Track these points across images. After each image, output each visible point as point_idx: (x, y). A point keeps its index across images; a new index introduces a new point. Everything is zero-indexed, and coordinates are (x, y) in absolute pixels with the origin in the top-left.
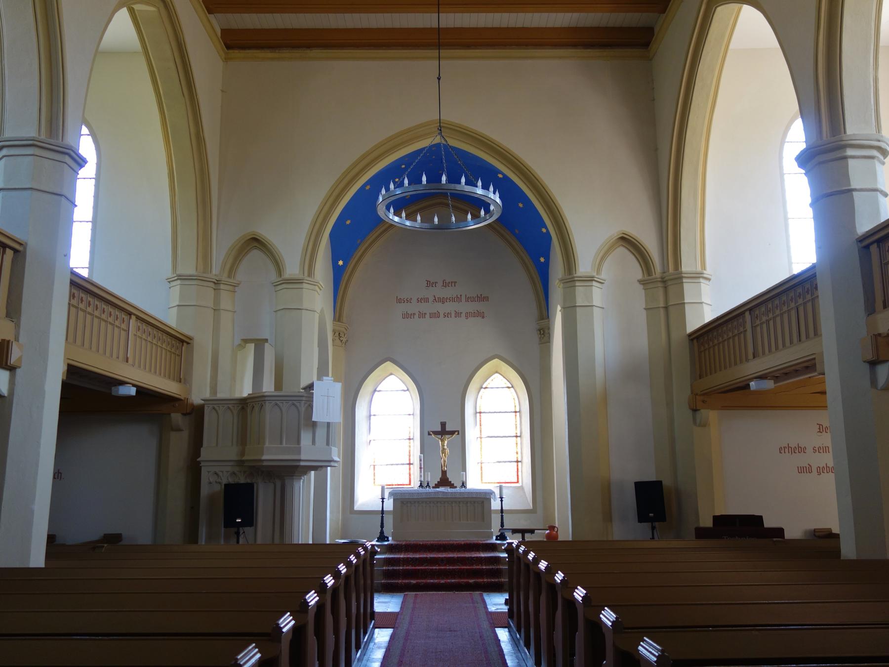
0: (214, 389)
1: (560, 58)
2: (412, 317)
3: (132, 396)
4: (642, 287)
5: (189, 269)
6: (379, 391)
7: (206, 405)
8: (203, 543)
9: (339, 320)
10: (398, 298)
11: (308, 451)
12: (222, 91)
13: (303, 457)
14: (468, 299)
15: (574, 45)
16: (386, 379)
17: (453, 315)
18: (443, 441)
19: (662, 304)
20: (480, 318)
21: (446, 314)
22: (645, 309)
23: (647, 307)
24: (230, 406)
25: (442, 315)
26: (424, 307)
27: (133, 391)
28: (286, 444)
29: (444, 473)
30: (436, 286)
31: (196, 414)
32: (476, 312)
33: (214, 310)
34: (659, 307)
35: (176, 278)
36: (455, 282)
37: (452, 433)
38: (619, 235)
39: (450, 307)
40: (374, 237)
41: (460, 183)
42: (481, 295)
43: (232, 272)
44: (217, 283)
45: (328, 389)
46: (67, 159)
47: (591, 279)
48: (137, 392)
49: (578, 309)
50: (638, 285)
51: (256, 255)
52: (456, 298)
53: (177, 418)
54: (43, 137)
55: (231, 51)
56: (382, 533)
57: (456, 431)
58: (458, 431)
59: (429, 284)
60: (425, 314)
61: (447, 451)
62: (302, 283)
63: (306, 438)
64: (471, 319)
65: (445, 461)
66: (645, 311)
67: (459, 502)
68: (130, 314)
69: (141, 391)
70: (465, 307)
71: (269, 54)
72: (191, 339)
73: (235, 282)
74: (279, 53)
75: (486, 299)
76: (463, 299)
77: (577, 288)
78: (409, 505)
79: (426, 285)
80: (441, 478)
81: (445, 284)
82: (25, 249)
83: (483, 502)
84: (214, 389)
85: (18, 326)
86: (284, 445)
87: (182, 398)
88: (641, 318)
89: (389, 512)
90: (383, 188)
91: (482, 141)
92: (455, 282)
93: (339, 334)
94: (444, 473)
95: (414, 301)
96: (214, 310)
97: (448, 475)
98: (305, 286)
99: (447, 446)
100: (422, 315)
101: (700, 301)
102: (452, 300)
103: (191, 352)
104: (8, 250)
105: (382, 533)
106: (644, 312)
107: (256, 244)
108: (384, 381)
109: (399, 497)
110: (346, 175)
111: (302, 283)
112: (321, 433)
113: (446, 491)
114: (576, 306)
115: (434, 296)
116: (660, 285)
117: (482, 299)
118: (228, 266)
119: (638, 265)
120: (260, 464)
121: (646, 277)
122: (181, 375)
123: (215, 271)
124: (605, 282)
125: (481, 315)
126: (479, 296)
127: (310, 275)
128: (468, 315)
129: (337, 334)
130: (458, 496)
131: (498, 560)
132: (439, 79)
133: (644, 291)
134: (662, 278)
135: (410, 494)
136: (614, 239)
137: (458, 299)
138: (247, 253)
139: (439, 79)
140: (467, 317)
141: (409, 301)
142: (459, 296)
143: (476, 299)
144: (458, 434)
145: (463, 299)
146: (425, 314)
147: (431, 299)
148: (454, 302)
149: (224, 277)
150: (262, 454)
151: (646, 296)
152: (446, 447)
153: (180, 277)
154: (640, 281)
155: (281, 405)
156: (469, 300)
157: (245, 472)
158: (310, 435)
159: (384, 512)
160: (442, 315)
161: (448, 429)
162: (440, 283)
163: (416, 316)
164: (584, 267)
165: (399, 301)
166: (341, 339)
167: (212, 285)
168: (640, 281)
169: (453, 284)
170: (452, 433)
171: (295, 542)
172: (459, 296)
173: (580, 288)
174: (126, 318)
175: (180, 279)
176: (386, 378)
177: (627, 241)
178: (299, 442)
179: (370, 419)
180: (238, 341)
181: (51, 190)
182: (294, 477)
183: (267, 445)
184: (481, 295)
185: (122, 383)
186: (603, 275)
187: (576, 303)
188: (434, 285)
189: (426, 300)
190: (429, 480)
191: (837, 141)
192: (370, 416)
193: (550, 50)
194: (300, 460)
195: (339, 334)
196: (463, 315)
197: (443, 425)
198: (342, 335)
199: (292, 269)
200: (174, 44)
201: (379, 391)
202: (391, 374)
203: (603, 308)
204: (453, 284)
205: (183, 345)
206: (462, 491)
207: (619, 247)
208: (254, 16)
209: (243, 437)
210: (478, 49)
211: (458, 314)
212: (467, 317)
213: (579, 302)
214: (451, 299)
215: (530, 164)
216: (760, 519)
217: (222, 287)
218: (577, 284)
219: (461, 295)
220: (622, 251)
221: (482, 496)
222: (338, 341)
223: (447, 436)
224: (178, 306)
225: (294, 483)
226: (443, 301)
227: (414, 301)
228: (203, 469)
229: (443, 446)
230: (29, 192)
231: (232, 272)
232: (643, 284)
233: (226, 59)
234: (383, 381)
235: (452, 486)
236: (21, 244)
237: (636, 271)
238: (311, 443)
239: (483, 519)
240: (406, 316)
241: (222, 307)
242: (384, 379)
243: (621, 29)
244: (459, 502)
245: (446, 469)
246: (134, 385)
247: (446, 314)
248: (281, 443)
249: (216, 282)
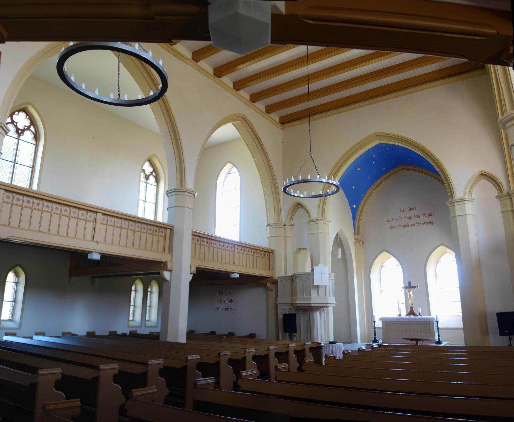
0: (286, 272)
1: (435, 86)
2: (395, 228)
3: (238, 278)
4: (498, 200)
5: (272, 221)
6: (384, 267)
7: (278, 280)
8: (281, 340)
9: (358, 234)
10: (423, 214)
11: (315, 299)
12: (282, 143)
13: (312, 302)
14: (423, 216)
15: (443, 78)
16: (387, 260)
17: (416, 225)
18: (409, 291)
19: (510, 209)
20: (430, 225)
21: (412, 225)
22: (501, 212)
23: (502, 211)
24: (288, 279)
25: (410, 225)
26: (400, 223)
27: (237, 276)
28: (306, 296)
29: (412, 308)
30: (405, 211)
31: (275, 282)
32: (428, 222)
33: (284, 237)
34: (508, 211)
35: (267, 226)
36: (415, 208)
37: (414, 287)
38: (478, 173)
39: (414, 221)
40: (370, 192)
41: (317, 178)
42: (430, 213)
43: (291, 219)
44: (284, 225)
45: (321, 270)
46: (187, 194)
47: (463, 200)
48: (239, 276)
49: (457, 218)
50: (495, 199)
51: (300, 210)
52: (416, 216)
53: (269, 285)
54: (179, 188)
55: (284, 125)
56: (375, 338)
57: (417, 286)
58: (418, 286)
59: (402, 210)
60: (401, 226)
61: (413, 296)
62: (318, 221)
63: (314, 293)
64: (425, 226)
65: (411, 302)
66: (501, 214)
67: (417, 324)
68: (166, 228)
69: (241, 275)
70: (422, 220)
71: (299, 122)
72: (274, 251)
73: (292, 224)
74: (302, 120)
75: (433, 214)
76: (420, 216)
77: (466, 204)
78: (390, 325)
79: (400, 211)
80: (410, 311)
81: (410, 209)
82: (174, 228)
83: (429, 324)
84: (286, 272)
85: (172, 255)
86: (305, 296)
87: (270, 276)
88: (499, 218)
89: (379, 328)
90: (298, 190)
91: (396, 138)
92: (415, 208)
93: (358, 240)
94: (412, 308)
95: (395, 220)
96: (284, 237)
97: (414, 310)
98: (319, 222)
99: (412, 294)
100: (399, 227)
101: (464, 214)
102: (414, 217)
103: (274, 257)
104: (167, 229)
105: (375, 338)
106: (501, 215)
107: (300, 206)
108: (386, 261)
109: (384, 321)
110: (334, 169)
111: (318, 221)
112: (321, 291)
113: (408, 318)
114: (456, 216)
115: (405, 216)
116: (507, 197)
117: (431, 214)
118: (289, 217)
119: (496, 189)
120: (310, 305)
121: (500, 194)
122: (271, 267)
123: (283, 220)
124: (475, 200)
125: (431, 223)
126: (429, 213)
127: (322, 217)
128: (424, 224)
129: (357, 240)
130: (424, 321)
131: (350, 353)
132: (310, 130)
133: (499, 202)
134: (508, 193)
135: (389, 319)
136: (476, 176)
137: (418, 216)
138: (297, 210)
139: (310, 130)
140: (423, 225)
141: (392, 220)
142: (418, 215)
143: (428, 215)
144: (418, 288)
145: (420, 216)
146: (401, 226)
147: (403, 218)
148: (416, 218)
149: (467, 197)
150: (296, 301)
151: (501, 204)
152: (411, 295)
153: (268, 225)
154: (496, 197)
155: (302, 278)
156: (424, 216)
157: (295, 308)
158: (316, 292)
159: (376, 328)
160: (410, 225)
161: (412, 285)
162: (407, 209)
163: (397, 227)
164: (458, 194)
165: (387, 221)
166: (359, 242)
167: (283, 227)
168: (496, 197)
169: (414, 209)
170: (414, 287)
171: (316, 341)
172: (429, 213)
173: (458, 206)
174: (163, 230)
175: (269, 226)
176: (387, 259)
177: (484, 175)
178: (311, 295)
179: (381, 281)
180: (295, 250)
181: (180, 206)
182: (314, 311)
183: (298, 296)
184: (430, 213)
185: (233, 273)
186: (473, 196)
187: (456, 214)
188: (404, 211)
189: (401, 219)
190: (420, 312)
191: (511, 115)
192: (381, 279)
193: (348, 107)
194: (311, 303)
195: (358, 240)
196: (421, 224)
197: (409, 283)
198: (359, 240)
199: (314, 215)
200: (251, 132)
201: (384, 267)
202: (446, 253)
203: (474, 215)
204: (414, 209)
205: (270, 254)
206: (400, 318)
207: (481, 179)
208: (289, 109)
209: (293, 293)
210: (392, 94)
211: (418, 224)
212: (423, 225)
213: (458, 213)
214: (414, 217)
215: (424, 145)
216: (116, 332)
217: (287, 227)
218: (456, 204)
219: (419, 214)
220: (484, 182)
221: (428, 321)
222: (357, 244)
223: (411, 289)
224: (269, 237)
225: (314, 314)
226: (410, 218)
227: (395, 220)
228: (279, 307)
229: (410, 294)
230: (174, 208)
231: (291, 219)
232: (499, 198)
233: (283, 129)
234: (386, 261)
235: (415, 315)
236: (172, 227)
237: (495, 192)
238: (317, 295)
239: (430, 333)
240: (392, 228)
241: (287, 235)
242: (386, 260)
243: (438, 71)
244: (417, 324)
245: (412, 306)
246: (238, 273)
247: (412, 225)
248: (304, 296)
249: (284, 225)
